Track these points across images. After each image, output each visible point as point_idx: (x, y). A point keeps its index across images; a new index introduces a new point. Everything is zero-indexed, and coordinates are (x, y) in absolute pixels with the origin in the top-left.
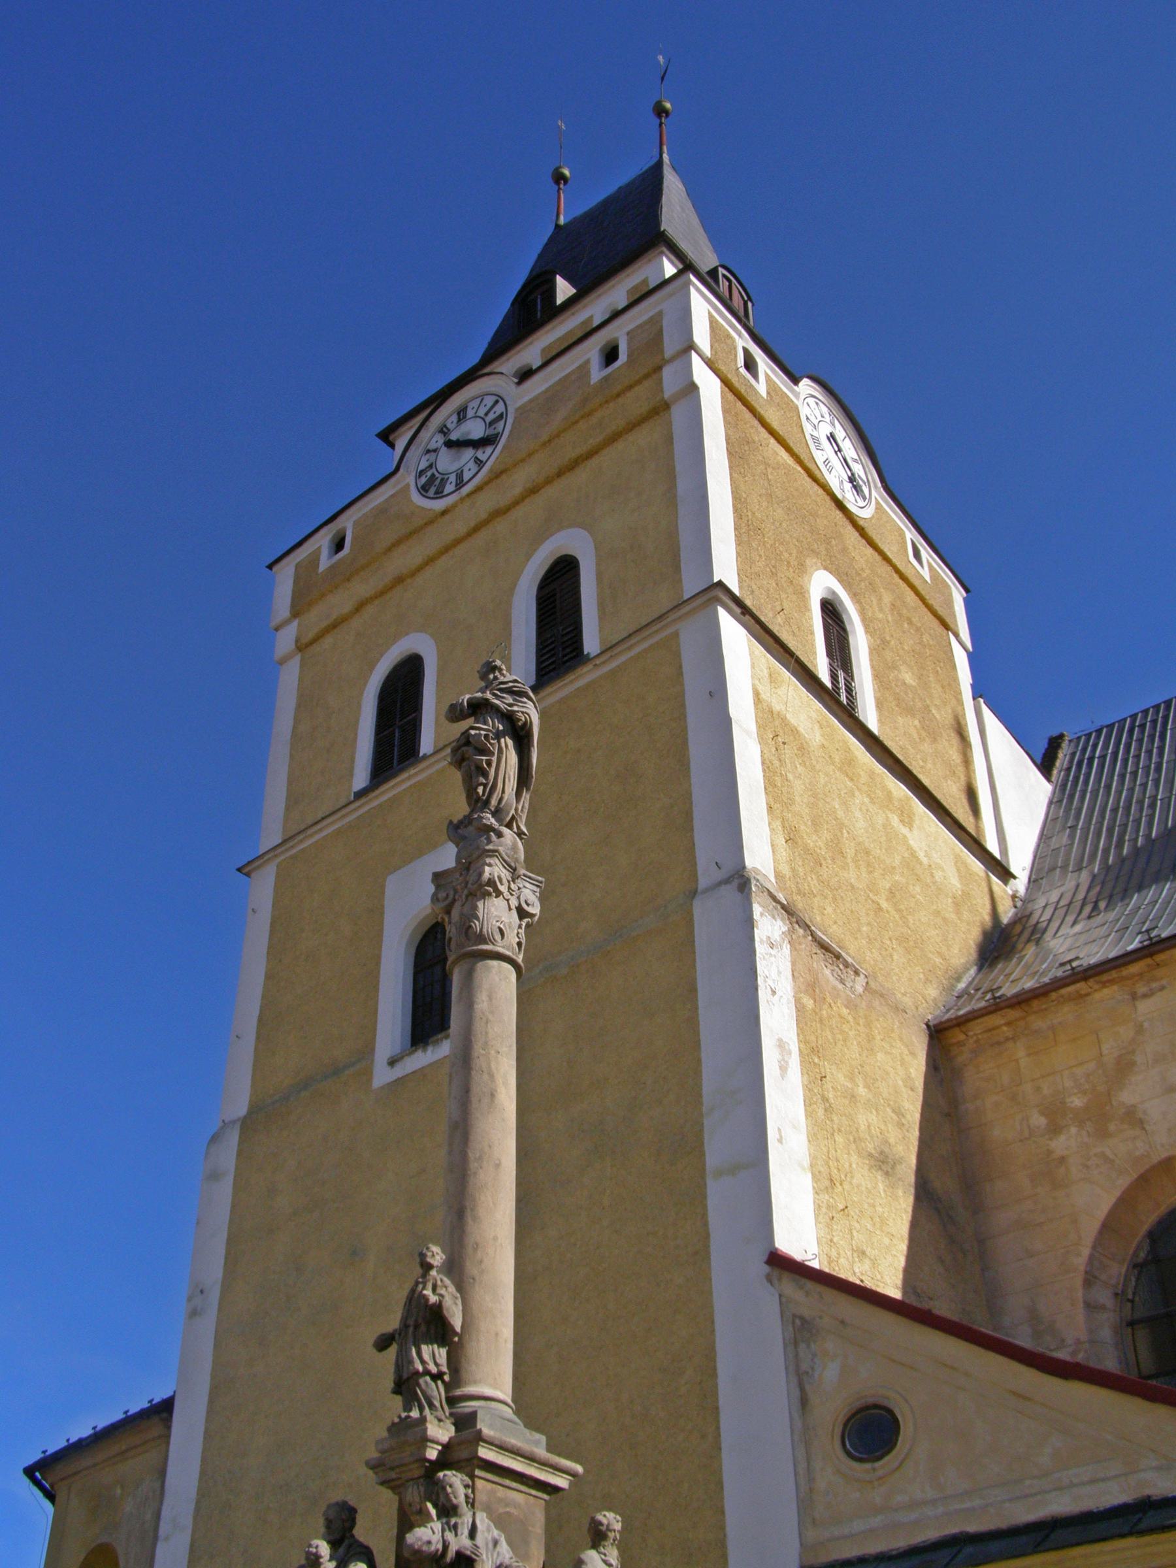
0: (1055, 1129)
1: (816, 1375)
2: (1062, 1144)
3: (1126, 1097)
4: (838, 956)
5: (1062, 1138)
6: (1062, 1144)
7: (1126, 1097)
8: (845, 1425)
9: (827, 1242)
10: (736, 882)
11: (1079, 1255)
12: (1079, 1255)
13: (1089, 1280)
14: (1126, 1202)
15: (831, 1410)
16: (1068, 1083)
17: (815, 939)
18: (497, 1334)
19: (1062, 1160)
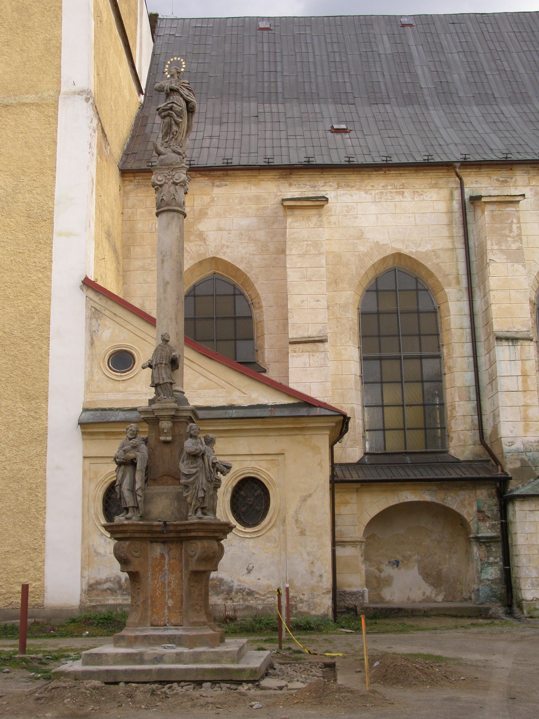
1: (99, 333)
4: (106, 136)
7: (201, 227)
8: (110, 356)
9: (95, 273)
10: (84, 96)
15: (106, 349)
17: (102, 126)
18: (448, 436)
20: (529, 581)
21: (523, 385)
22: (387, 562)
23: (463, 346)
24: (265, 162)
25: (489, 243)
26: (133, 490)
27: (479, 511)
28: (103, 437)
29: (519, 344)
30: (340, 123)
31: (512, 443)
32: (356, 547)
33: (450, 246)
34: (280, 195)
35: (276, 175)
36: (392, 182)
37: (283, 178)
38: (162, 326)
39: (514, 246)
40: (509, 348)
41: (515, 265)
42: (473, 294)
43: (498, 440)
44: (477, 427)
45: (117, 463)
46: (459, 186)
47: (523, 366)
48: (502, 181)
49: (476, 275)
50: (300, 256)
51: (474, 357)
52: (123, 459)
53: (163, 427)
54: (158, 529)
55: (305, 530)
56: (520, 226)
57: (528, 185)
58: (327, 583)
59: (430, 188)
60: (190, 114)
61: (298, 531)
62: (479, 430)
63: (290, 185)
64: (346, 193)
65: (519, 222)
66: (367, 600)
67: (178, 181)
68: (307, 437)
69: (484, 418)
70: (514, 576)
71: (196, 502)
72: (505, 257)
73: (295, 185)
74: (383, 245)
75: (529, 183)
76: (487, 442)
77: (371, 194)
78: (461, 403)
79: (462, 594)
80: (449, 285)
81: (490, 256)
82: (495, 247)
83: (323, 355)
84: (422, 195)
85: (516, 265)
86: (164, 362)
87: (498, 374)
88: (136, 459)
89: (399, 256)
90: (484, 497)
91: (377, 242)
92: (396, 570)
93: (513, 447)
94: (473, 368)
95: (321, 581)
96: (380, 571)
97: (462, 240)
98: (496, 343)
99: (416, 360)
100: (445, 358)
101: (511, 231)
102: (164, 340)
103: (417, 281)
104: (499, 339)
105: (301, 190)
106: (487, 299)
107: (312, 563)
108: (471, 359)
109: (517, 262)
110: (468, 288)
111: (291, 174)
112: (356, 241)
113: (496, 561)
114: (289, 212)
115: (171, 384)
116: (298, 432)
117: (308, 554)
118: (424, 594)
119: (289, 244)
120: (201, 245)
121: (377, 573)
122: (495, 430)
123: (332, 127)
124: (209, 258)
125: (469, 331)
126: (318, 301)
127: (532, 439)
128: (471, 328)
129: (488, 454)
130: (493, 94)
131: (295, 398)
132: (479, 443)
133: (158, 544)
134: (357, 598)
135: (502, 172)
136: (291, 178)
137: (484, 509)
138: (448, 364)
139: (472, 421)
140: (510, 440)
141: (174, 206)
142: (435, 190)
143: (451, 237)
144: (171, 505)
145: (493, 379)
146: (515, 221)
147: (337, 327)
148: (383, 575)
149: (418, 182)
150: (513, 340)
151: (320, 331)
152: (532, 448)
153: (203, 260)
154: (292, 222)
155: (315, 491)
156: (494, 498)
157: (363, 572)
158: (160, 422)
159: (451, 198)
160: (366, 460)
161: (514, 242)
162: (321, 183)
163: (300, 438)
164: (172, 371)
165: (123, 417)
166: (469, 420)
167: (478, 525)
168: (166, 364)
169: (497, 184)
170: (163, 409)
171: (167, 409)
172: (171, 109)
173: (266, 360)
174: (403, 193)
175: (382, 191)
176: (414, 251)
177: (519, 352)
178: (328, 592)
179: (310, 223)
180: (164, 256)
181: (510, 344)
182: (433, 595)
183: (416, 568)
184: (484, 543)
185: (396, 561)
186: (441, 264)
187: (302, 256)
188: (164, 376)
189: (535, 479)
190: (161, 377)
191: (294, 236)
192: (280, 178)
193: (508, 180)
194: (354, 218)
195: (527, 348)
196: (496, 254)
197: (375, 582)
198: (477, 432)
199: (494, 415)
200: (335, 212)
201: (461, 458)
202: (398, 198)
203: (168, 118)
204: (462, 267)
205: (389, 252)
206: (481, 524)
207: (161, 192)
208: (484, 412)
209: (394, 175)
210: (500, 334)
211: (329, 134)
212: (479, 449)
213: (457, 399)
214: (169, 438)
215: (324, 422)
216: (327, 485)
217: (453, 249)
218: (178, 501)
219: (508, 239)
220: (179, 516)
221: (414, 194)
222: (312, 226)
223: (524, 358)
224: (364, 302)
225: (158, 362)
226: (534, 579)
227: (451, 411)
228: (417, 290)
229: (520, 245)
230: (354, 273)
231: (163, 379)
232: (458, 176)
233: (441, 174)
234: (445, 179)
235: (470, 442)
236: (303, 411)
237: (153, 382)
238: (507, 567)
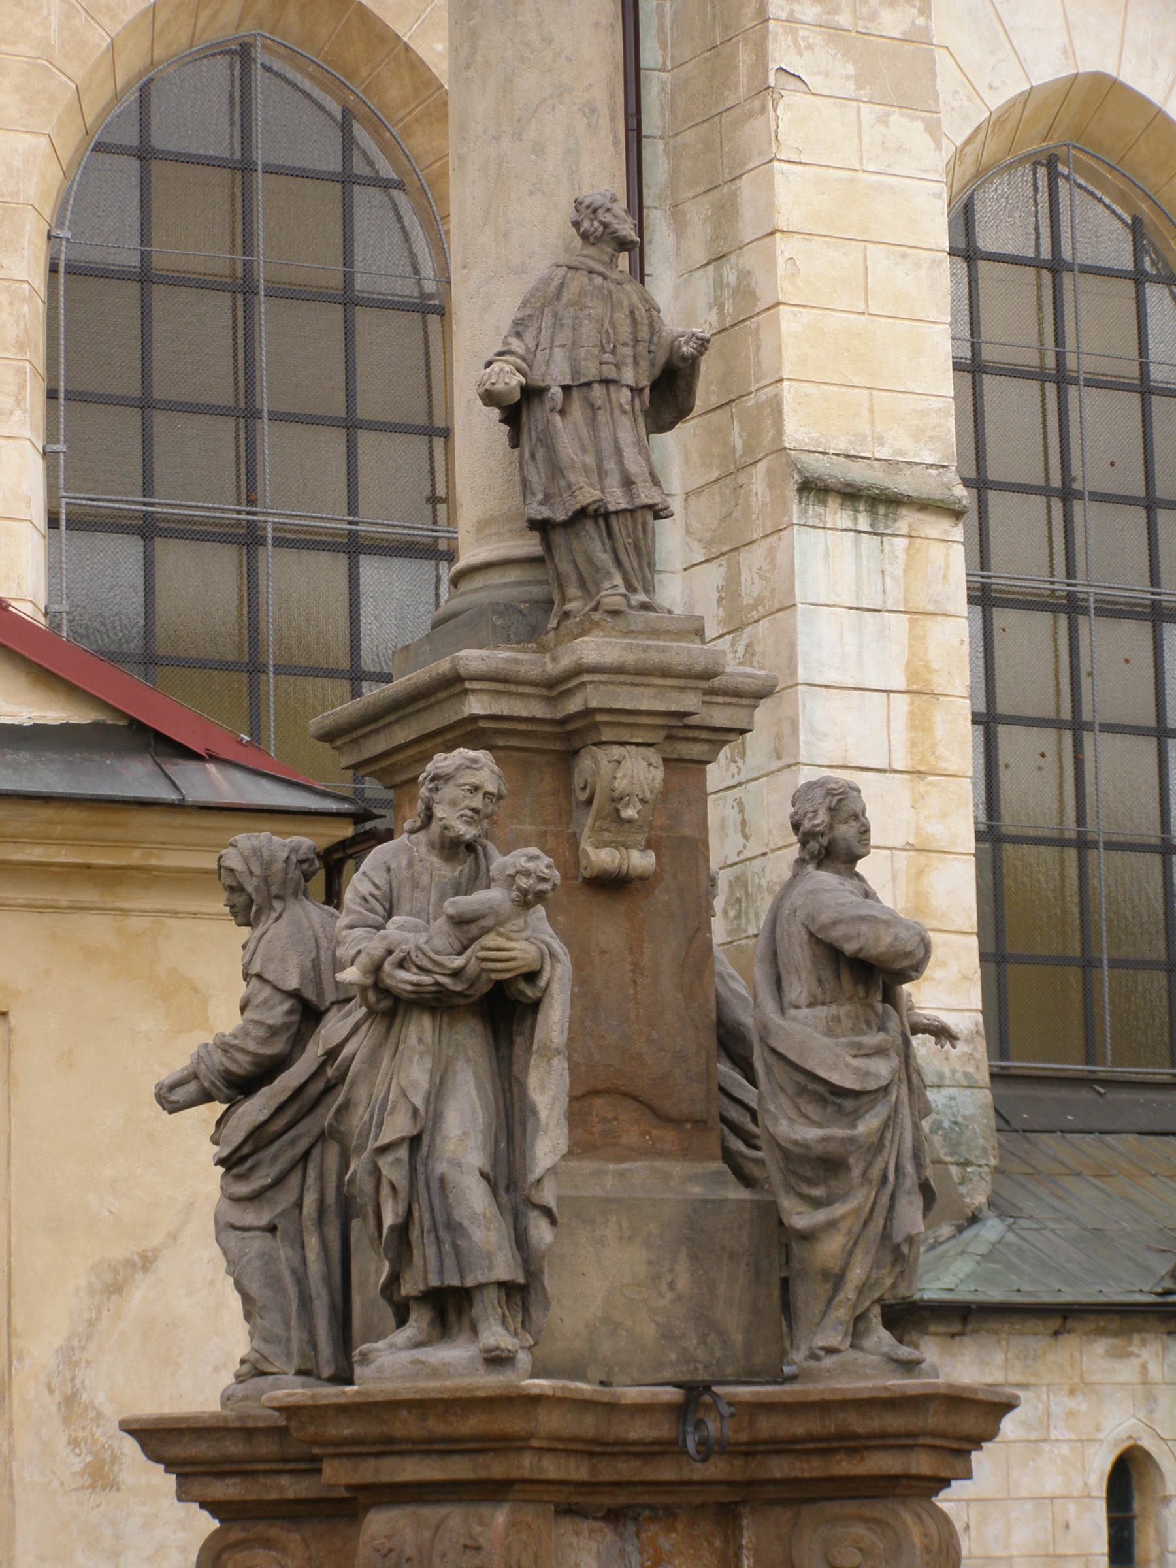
21: (913, 744)
26: (507, 1178)
29: (902, 526)
38: (539, 150)
40: (857, 544)
41: (896, 117)
47: (916, 640)
49: (660, 145)
52: (456, 974)
53: (621, 785)
54: (639, 1430)
55: (114, 1458)
61: (77, 1464)
68: (136, 924)
71: (877, 1264)
72: (850, 69)
85: (896, 118)
87: (802, 675)
88: (532, 977)
98: (795, 508)
99: (324, 557)
104: (813, 488)
109: (905, 105)
116: (90, 896)
133: (586, 1525)
144: (656, 1278)
150: (876, 502)
152: (946, 1069)
155: (173, 1236)
163: (97, 928)
168: (636, 391)
170: (640, 674)
171: (664, 672)
177: (899, 572)
181: (863, 523)
189: (960, 1230)
190: (610, 465)
195: (936, 552)
196: (810, 47)
210: (820, 467)
214: (641, 860)
218: (694, 1258)
220: (700, 1353)
223: (921, 602)
224: (75, 203)
225: (591, 371)
229: (920, 21)
230: (54, 38)
231: (628, 483)
236: (137, 777)
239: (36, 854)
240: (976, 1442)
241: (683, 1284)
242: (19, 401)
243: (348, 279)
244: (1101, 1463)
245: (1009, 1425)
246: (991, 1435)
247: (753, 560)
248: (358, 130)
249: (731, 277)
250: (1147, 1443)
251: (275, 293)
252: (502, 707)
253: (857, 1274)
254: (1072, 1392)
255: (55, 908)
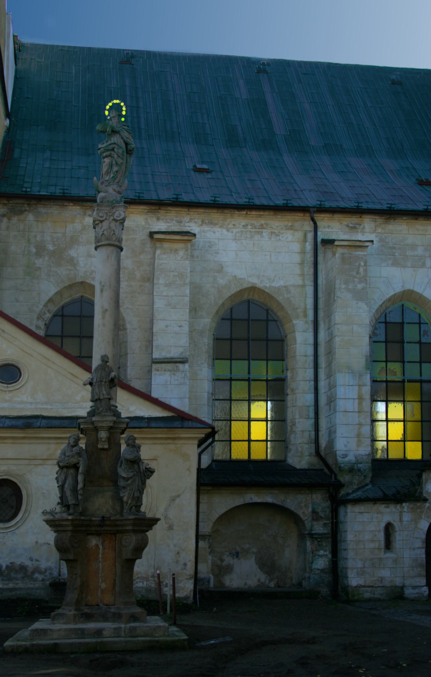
0: (38, 254)
2: (39, 262)
3: (73, 253)
5: (41, 260)
6: (39, 262)
7: (73, 253)
11: (37, 307)
12: (37, 307)
13: (39, 317)
14: (59, 293)
16: (49, 238)
19: (39, 268)
20: (355, 571)
22: (228, 553)
23: (305, 372)
24: (136, 196)
25: (338, 282)
27: (314, 512)
28: (11, 441)
30: (203, 163)
31: (345, 456)
32: (205, 540)
33: (300, 283)
34: (148, 228)
35: (145, 209)
36: (253, 222)
37: (151, 212)
39: (359, 286)
42: (318, 326)
43: (334, 454)
44: (313, 441)
45: (59, 466)
46: (312, 229)
48: (352, 228)
50: (166, 285)
51: (315, 381)
52: (67, 463)
55: (173, 525)
56: (366, 269)
57: (374, 231)
58: (190, 570)
59: (287, 229)
60: (128, 155)
61: (166, 526)
62: (315, 443)
63: (158, 219)
64: (210, 230)
65: (365, 265)
66: (212, 585)
67: (118, 219)
69: (321, 434)
70: (341, 566)
73: (162, 219)
74: (240, 279)
75: (376, 230)
76: (322, 453)
77: (232, 232)
78: (301, 420)
79: (292, 580)
80: (297, 317)
81: (338, 294)
82: (343, 286)
83: (183, 375)
84: (279, 235)
85: (360, 303)
86: (104, 380)
87: (337, 397)
89: (253, 289)
90: (318, 500)
91: (235, 276)
92: (236, 560)
93: (346, 459)
94: (313, 391)
95: (185, 569)
96: (222, 561)
97: (312, 278)
100: (289, 381)
101: (358, 273)
102: (103, 361)
103: (268, 313)
105: (168, 224)
106: (332, 331)
107: (178, 553)
108: (312, 383)
110: (314, 321)
111: (159, 209)
112: (216, 274)
113: (325, 553)
114: (158, 244)
115: (110, 399)
116: (170, 441)
117: (175, 546)
118: (259, 580)
119: (157, 273)
120: (71, 270)
121: (219, 562)
122: (331, 443)
123: (195, 166)
124: (78, 282)
125: (312, 358)
126: (181, 326)
127: (363, 453)
128: (314, 356)
129: (321, 463)
130: (341, 146)
131: (174, 413)
132: (314, 454)
134: (204, 583)
135: (352, 219)
136: (159, 212)
137: (318, 510)
138: (291, 387)
139: (309, 436)
140: (344, 453)
141: (114, 241)
142: (291, 232)
143: (302, 275)
145: (331, 400)
146: (362, 264)
147: (194, 350)
148: (224, 564)
149: (276, 222)
151: (182, 353)
153: (73, 284)
154: (161, 254)
156: (327, 501)
157: (210, 561)
158: (99, 432)
159: (305, 240)
160: (214, 466)
161: (360, 282)
162: (187, 219)
164: (111, 388)
165: (10, 424)
166: (306, 434)
167: (312, 524)
168: (105, 382)
169: (347, 229)
172: (113, 150)
173: (129, 377)
174: (262, 232)
175: (243, 230)
176: (268, 286)
178: (190, 578)
179: (177, 256)
180: (103, 286)
182: (267, 582)
183: (253, 558)
184: (316, 538)
185: (236, 552)
186: (292, 299)
187: (168, 285)
188: (104, 392)
191: (162, 267)
192: (148, 212)
193: (357, 226)
194: (216, 253)
197: (221, 570)
198: (313, 446)
199: (330, 431)
200: (198, 247)
201: (298, 467)
202: (257, 237)
203: (110, 158)
204: (310, 302)
205: (245, 286)
206: (315, 523)
207: (102, 227)
208: (320, 429)
209: (254, 216)
211: (192, 172)
212: (315, 460)
213: (297, 417)
214: (106, 446)
215: (194, 434)
216: (194, 487)
217: (303, 286)
219: (355, 279)
221: (272, 234)
222: (179, 258)
226: (359, 569)
227: (291, 427)
228: (267, 320)
232: (313, 220)
233: (297, 217)
234: (300, 222)
235: (307, 453)
237: (93, 396)
238: (335, 559)
239: (160, 436)
240: (154, 525)
241: (110, 503)
242: (205, 361)
243: (267, 337)
244: (383, 525)
245: (159, 523)
246: (156, 524)
247: (332, 378)
248: (269, 311)
249: (330, 332)
250: (392, 522)
251: (252, 340)
252: (86, 426)
253: (129, 502)
254: (377, 513)
255: (165, 444)
